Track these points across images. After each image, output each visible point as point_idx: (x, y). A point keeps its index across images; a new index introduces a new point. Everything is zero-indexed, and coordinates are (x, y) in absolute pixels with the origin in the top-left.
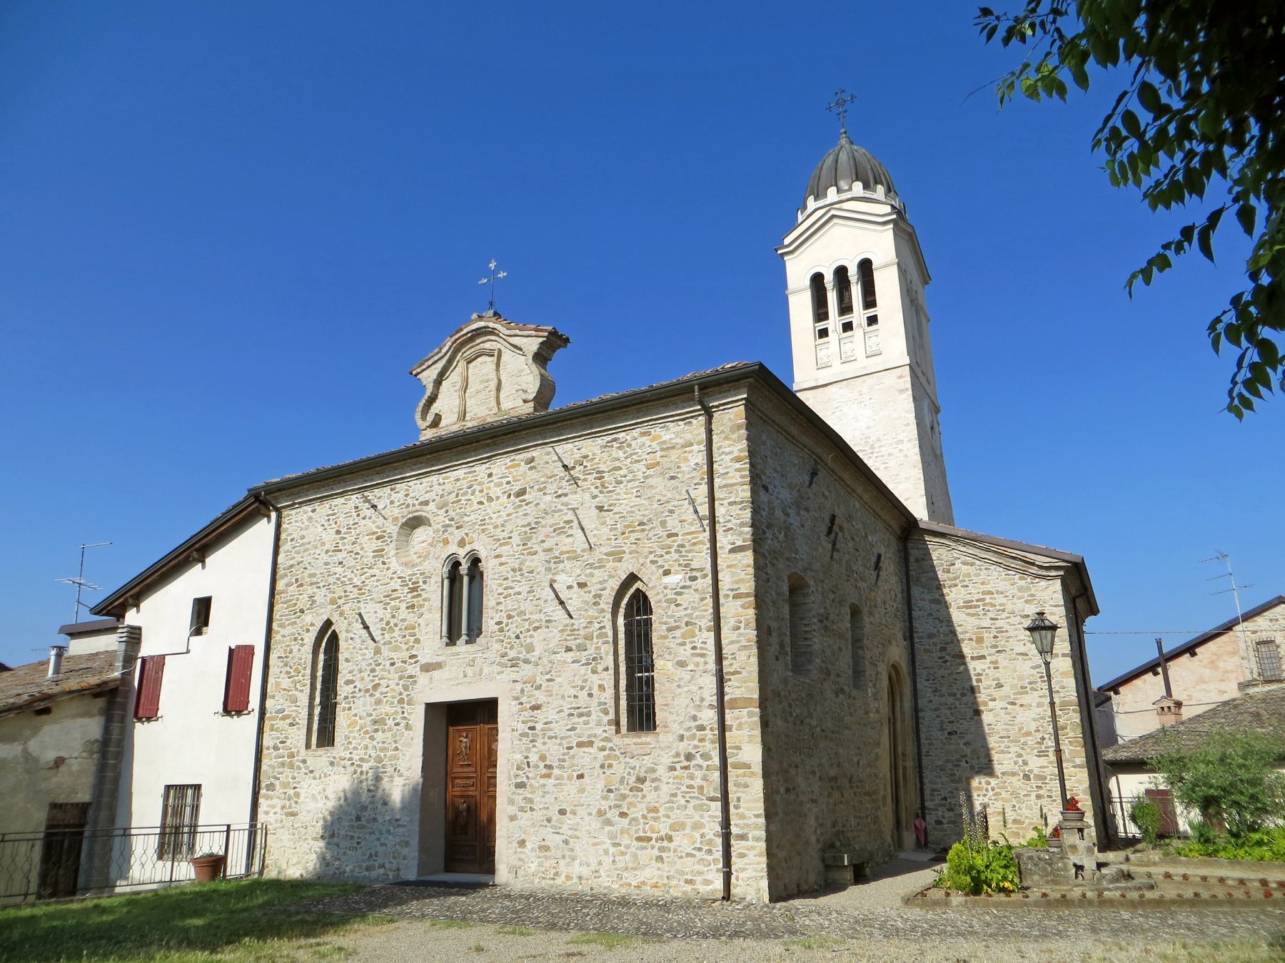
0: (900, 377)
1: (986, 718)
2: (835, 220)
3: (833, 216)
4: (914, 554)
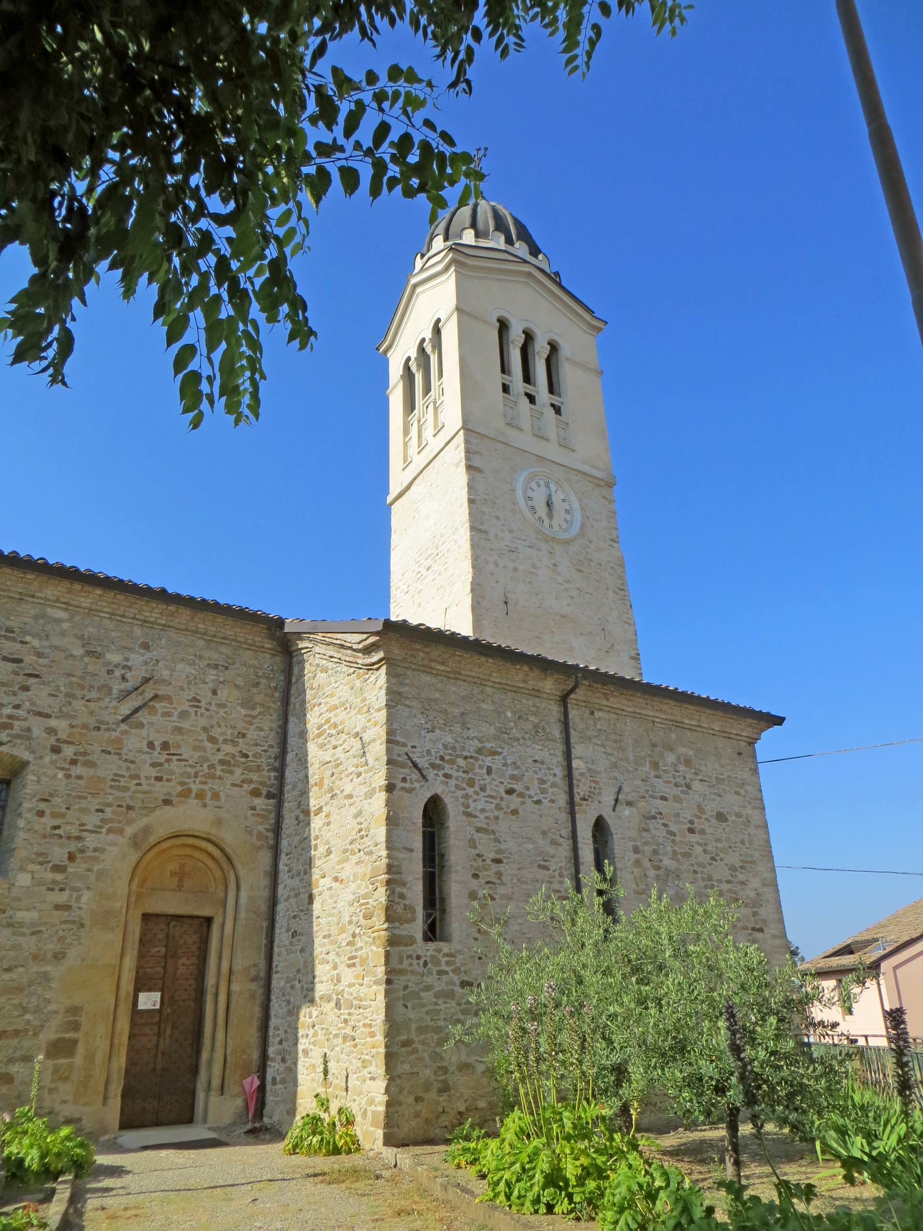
0: (457, 448)
1: (317, 906)
2: (419, 290)
3: (415, 286)
4: (296, 670)
